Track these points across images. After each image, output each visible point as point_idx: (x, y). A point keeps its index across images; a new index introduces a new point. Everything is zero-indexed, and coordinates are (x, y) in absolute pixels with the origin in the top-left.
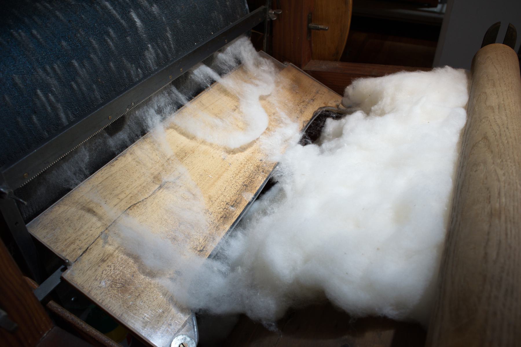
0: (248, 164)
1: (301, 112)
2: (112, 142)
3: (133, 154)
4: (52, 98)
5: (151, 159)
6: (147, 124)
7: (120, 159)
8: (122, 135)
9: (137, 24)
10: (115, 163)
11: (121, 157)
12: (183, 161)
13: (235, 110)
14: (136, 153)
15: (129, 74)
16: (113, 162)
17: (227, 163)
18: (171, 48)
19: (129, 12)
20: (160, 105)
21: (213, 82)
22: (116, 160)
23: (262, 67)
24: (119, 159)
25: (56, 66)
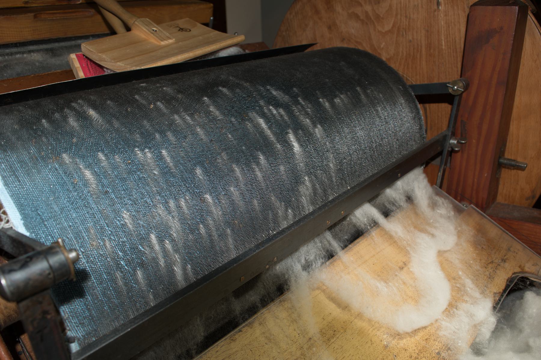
0: (420, 358)
1: (491, 278)
2: (237, 306)
3: (263, 325)
4: (168, 245)
5: (287, 336)
6: (289, 286)
7: (245, 330)
8: (253, 297)
9: (295, 149)
10: (237, 336)
11: (246, 328)
12: (329, 344)
13: (403, 268)
14: (267, 323)
15: (276, 216)
16: (235, 335)
17: (390, 354)
18: (332, 181)
19: (287, 133)
20: (308, 259)
21: (375, 224)
22: (240, 331)
23: (438, 209)
24: (244, 330)
25: (183, 203)
